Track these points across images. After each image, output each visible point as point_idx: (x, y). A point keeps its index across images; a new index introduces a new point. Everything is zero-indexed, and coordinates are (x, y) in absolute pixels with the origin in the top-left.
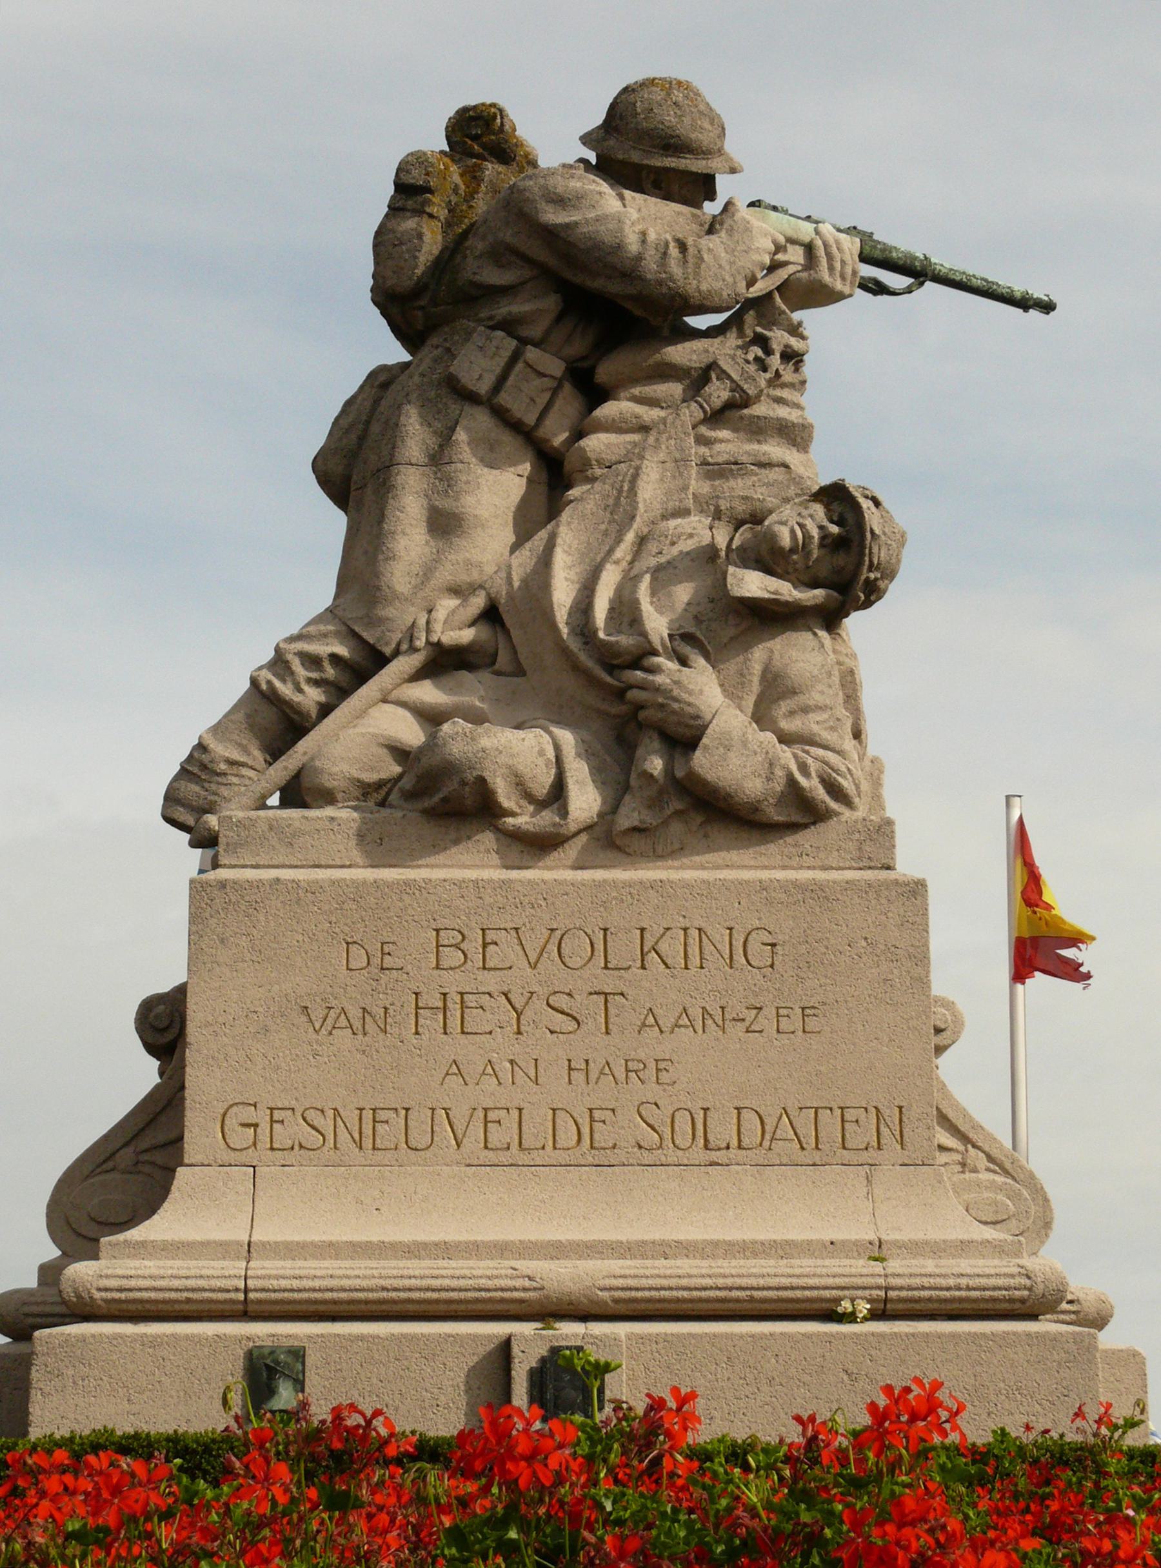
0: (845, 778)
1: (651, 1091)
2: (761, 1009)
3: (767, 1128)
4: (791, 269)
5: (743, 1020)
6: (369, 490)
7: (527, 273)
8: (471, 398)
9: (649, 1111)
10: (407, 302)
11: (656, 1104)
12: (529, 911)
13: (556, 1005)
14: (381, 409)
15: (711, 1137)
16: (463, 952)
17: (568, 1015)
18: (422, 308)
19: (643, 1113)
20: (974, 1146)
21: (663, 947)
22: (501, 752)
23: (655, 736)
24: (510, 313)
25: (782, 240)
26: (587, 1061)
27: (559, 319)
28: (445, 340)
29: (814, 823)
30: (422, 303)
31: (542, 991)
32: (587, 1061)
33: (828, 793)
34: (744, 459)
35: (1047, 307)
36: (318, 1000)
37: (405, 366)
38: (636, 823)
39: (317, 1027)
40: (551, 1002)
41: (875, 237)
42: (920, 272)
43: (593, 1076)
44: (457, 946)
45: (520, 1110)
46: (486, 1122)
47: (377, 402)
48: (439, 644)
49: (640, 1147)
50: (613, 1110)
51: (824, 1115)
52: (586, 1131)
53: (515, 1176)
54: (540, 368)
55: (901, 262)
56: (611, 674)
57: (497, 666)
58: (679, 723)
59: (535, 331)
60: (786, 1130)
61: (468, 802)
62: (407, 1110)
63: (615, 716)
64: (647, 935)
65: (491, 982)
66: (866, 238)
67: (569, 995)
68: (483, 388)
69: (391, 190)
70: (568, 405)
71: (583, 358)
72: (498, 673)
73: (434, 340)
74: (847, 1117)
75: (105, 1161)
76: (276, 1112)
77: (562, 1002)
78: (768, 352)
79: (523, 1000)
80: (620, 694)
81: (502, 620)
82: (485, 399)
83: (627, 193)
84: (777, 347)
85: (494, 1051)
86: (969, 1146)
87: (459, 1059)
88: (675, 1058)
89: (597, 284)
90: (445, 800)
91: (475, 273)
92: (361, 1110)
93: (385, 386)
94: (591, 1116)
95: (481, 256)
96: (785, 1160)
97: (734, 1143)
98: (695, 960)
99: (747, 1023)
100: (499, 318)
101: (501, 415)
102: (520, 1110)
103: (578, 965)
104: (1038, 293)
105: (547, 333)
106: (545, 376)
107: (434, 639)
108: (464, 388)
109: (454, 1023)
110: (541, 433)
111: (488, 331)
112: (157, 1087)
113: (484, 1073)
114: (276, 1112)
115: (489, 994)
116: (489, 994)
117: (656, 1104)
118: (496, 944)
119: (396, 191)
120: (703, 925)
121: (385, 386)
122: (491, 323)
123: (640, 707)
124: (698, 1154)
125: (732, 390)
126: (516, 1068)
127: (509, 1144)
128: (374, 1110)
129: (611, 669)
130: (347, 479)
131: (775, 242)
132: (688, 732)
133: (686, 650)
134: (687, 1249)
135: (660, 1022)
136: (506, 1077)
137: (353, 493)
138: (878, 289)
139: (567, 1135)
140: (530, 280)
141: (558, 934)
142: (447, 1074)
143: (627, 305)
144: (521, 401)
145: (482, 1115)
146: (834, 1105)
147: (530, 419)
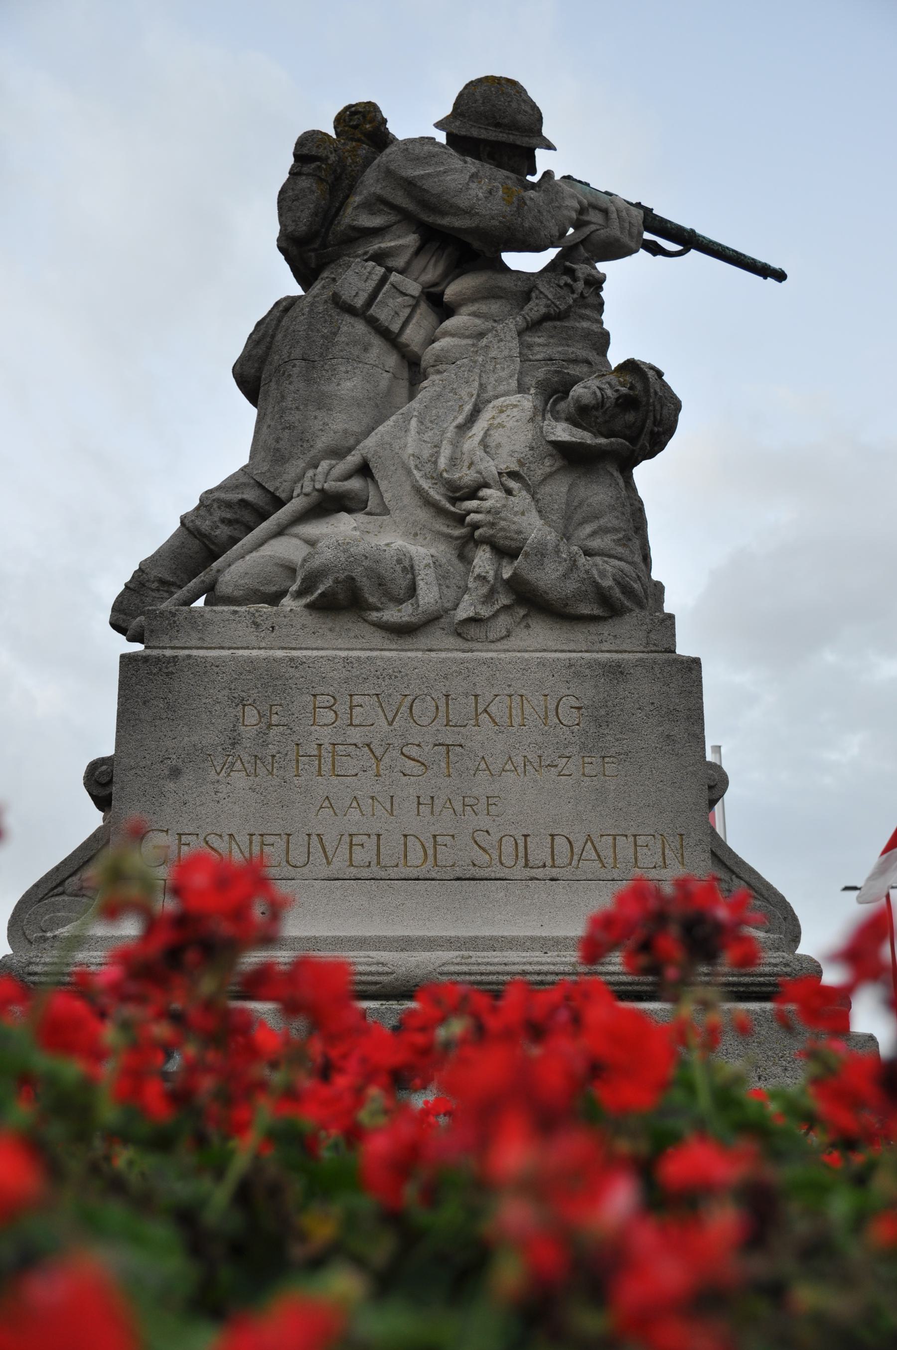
0: (635, 582)
1: (484, 822)
2: (569, 757)
3: (575, 850)
4: (593, 227)
5: (556, 766)
6: (273, 384)
7: (393, 218)
8: (349, 310)
9: (481, 837)
10: (306, 247)
11: (487, 832)
12: (387, 681)
13: (408, 753)
14: (283, 323)
15: (530, 858)
16: (335, 712)
17: (418, 761)
18: (314, 250)
19: (477, 839)
20: (738, 877)
21: (493, 709)
22: (366, 558)
23: (487, 548)
24: (380, 248)
25: (585, 201)
26: (432, 798)
27: (418, 252)
28: (332, 273)
29: (611, 617)
30: (316, 246)
31: (397, 742)
32: (432, 798)
33: (623, 593)
34: (557, 356)
35: (780, 276)
36: (220, 749)
37: (300, 297)
38: (472, 614)
39: (218, 770)
40: (404, 751)
41: (654, 212)
42: (689, 240)
43: (437, 810)
44: (330, 707)
45: (379, 836)
46: (351, 845)
47: (279, 321)
48: (322, 491)
49: (474, 865)
50: (453, 836)
51: (621, 840)
52: (430, 852)
53: (374, 887)
54: (402, 289)
55: (674, 232)
56: (454, 505)
57: (368, 509)
58: (506, 538)
59: (400, 262)
60: (590, 853)
61: (341, 597)
62: (289, 835)
63: (457, 538)
64: (480, 699)
65: (356, 735)
66: (648, 211)
67: (419, 745)
68: (359, 302)
69: (291, 160)
70: (424, 317)
71: (435, 285)
72: (369, 514)
73: (325, 274)
74: (639, 842)
75: (56, 887)
76: (183, 837)
77: (413, 751)
78: (575, 280)
79: (382, 749)
80: (460, 520)
81: (372, 474)
82: (361, 311)
83: (468, 159)
84: (580, 274)
85: (358, 790)
86: (734, 877)
87: (331, 795)
88: (503, 795)
89: (446, 221)
90: (322, 595)
91: (353, 220)
92: (251, 835)
93: (287, 310)
94: (435, 841)
95: (358, 207)
96: (590, 876)
97: (549, 862)
98: (517, 720)
99: (560, 769)
100: (371, 252)
101: (373, 323)
102: (379, 836)
103: (427, 723)
104: (775, 264)
105: (409, 263)
106: (406, 295)
107: (318, 486)
108: (345, 302)
109: (326, 768)
110: (406, 337)
111: (363, 262)
112: (100, 828)
113: (350, 807)
114: (183, 837)
115: (355, 745)
116: (355, 745)
117: (487, 832)
118: (361, 706)
119: (295, 161)
120: (523, 692)
121: (287, 310)
122: (365, 257)
123: (476, 526)
124: (519, 871)
125: (547, 306)
126: (376, 803)
127: (370, 863)
128: (262, 835)
129: (454, 501)
130: (258, 379)
131: (580, 203)
132: (514, 544)
133: (513, 484)
134: (512, 943)
135: (491, 768)
136: (367, 810)
137: (262, 389)
138: (655, 250)
139: (415, 855)
140: (395, 223)
141: (410, 698)
142: (321, 808)
143: (468, 239)
144: (387, 311)
145: (348, 840)
146: (629, 833)
147: (395, 327)
